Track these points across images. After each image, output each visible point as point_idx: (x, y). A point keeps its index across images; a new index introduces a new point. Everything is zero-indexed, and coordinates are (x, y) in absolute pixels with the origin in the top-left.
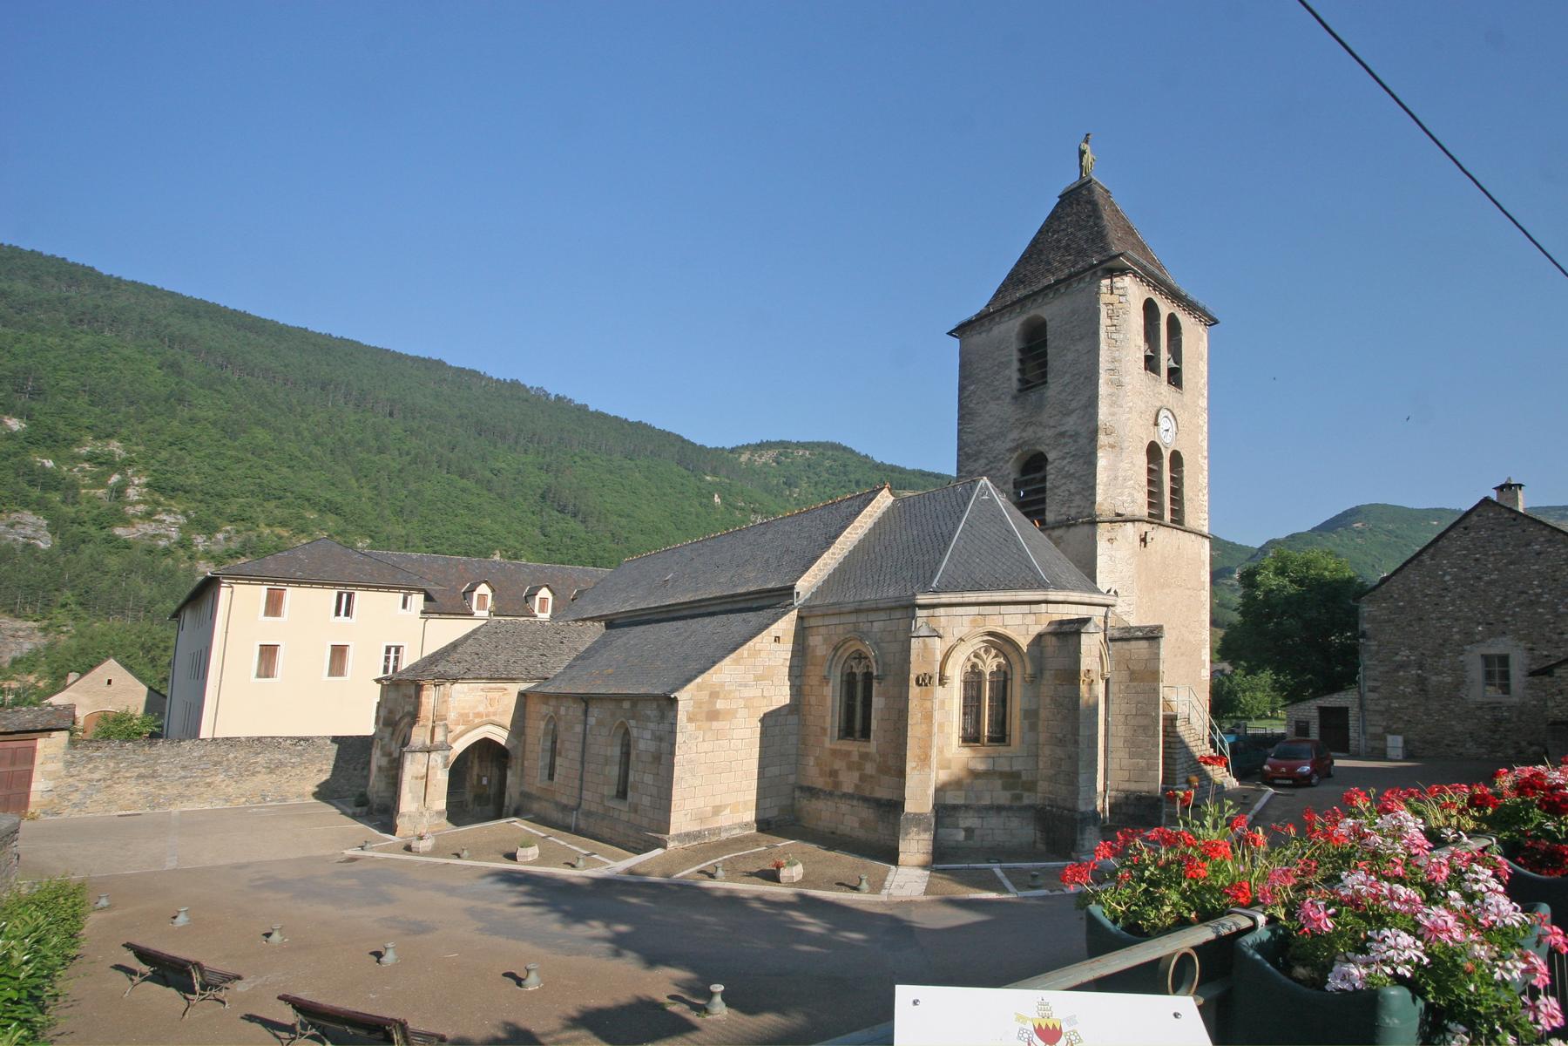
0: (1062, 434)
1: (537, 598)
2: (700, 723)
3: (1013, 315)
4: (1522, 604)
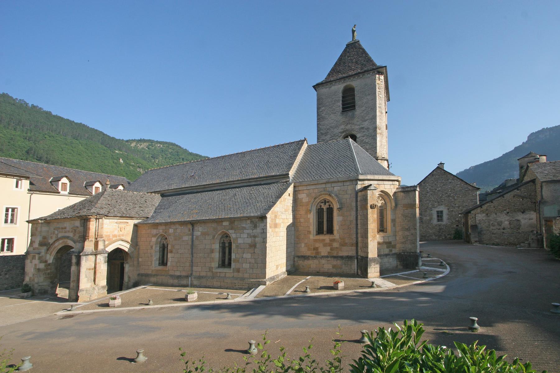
0: (363, 128)
1: (94, 187)
2: (272, 229)
3: (340, 83)
4: (446, 197)
